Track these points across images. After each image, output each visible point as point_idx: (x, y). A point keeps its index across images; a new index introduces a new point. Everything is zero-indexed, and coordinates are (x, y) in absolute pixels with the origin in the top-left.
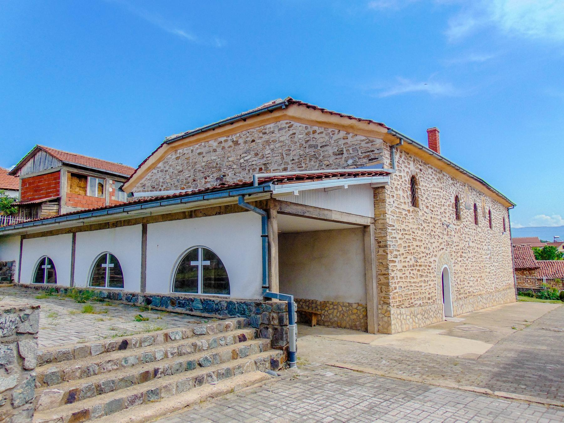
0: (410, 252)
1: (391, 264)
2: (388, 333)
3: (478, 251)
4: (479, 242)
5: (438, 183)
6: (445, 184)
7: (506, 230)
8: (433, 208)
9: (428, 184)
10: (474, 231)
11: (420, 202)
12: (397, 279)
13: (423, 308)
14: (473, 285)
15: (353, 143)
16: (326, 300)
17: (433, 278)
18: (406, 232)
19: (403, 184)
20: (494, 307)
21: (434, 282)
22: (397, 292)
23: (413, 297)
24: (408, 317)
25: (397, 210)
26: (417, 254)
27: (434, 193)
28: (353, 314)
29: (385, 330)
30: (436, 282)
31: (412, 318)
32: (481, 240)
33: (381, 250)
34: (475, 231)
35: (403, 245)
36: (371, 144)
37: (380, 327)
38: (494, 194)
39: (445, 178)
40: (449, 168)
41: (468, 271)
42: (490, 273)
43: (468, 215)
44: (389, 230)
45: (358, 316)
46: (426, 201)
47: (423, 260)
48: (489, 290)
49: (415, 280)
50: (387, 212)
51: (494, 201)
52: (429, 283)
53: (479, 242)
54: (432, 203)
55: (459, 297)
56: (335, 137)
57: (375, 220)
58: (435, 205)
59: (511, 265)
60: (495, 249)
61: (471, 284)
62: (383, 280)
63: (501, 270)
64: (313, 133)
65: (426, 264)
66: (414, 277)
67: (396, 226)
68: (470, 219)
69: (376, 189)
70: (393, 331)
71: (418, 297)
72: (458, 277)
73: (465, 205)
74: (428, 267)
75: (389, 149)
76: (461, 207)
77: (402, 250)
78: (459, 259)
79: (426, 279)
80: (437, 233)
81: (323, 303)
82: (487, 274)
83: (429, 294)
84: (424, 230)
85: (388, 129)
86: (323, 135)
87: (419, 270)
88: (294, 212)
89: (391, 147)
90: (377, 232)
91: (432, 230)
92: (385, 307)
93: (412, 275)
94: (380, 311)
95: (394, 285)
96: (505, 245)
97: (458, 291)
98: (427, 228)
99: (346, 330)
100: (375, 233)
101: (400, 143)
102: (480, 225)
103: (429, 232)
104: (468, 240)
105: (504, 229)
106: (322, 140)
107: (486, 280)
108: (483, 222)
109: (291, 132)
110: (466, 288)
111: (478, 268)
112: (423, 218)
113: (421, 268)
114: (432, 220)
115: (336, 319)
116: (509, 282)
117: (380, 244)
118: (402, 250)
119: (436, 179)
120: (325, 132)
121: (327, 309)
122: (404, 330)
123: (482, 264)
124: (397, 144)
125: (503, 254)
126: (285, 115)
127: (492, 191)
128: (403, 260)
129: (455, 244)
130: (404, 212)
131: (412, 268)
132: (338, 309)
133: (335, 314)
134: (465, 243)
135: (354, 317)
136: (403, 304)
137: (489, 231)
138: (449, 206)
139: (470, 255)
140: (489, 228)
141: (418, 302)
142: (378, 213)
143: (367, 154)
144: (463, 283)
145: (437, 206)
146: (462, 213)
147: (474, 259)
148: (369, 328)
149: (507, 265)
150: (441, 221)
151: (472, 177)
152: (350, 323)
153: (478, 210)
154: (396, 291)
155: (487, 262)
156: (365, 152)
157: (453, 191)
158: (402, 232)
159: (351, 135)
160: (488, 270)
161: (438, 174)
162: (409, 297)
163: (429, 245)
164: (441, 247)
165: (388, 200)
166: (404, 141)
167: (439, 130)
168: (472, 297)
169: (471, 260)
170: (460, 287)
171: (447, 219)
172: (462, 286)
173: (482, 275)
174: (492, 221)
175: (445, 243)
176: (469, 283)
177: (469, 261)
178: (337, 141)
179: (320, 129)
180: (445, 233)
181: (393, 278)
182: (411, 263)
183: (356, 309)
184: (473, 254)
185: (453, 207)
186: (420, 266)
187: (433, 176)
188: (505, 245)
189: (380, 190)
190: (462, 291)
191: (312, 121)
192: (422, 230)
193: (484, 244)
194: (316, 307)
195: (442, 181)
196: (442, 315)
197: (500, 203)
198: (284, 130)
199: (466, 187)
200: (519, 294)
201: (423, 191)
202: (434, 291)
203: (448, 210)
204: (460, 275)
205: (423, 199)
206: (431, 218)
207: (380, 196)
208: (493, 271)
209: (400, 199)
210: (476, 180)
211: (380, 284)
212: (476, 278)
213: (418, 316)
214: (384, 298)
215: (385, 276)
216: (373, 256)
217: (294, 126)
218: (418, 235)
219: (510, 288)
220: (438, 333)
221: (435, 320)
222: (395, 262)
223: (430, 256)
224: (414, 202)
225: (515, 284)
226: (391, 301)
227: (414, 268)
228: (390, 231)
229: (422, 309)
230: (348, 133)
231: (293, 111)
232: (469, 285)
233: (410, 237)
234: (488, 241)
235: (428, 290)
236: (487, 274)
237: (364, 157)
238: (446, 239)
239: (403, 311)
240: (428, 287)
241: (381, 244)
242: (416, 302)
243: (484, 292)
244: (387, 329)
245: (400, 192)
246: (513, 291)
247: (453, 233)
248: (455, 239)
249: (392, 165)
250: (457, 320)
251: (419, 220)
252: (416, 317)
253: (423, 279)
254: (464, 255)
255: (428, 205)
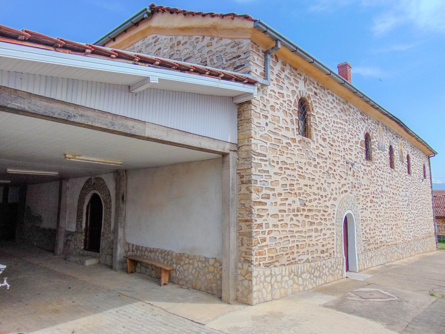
0: (293, 192)
1: (256, 207)
2: (248, 304)
3: (394, 196)
4: (394, 187)
5: (342, 114)
6: (351, 117)
7: (427, 178)
8: (334, 141)
9: (326, 112)
10: (389, 175)
11: (313, 133)
12: (268, 227)
13: (313, 264)
14: (387, 234)
15: (218, 49)
16: (182, 252)
17: (329, 226)
18: (288, 166)
19: (285, 105)
20: (411, 258)
21: (332, 231)
22: (267, 246)
23: (295, 250)
24: (286, 278)
25: (273, 136)
26: (305, 195)
27: (336, 125)
28: (209, 272)
29: (244, 299)
30: (335, 231)
31: (293, 279)
32: (397, 185)
33: (244, 187)
34: (391, 175)
35: (281, 182)
36: (237, 47)
37: (239, 294)
38: (413, 139)
39: (352, 110)
40: (355, 99)
41: (381, 219)
42: (407, 220)
43: (381, 157)
44: (256, 160)
45: (215, 276)
46: (323, 132)
47: (314, 203)
48: (406, 239)
49: (300, 229)
50: (253, 135)
51: (414, 147)
52: (324, 232)
53: (394, 187)
54: (331, 136)
55: (368, 248)
56: (199, 46)
57: (238, 148)
58: (336, 138)
59: (431, 212)
60: (413, 196)
61: (384, 232)
62: (245, 229)
63: (421, 218)
64: (178, 45)
65: (319, 208)
66: (300, 225)
67: (270, 156)
68: (385, 162)
69: (241, 105)
70: (255, 302)
71: (305, 250)
72: (367, 225)
73: (378, 144)
74: (322, 212)
75: (261, 54)
76: (373, 146)
77: (279, 189)
78: (369, 204)
79: (319, 228)
80: (338, 172)
81: (178, 255)
82: (404, 222)
83: (323, 246)
84: (318, 166)
85: (255, 21)
86: (187, 46)
87: (307, 216)
88: (41, 111)
89: (266, 53)
90: (240, 162)
91: (331, 168)
92: (246, 266)
93: (294, 222)
94: (239, 271)
95: (261, 236)
96: (425, 193)
97: (367, 241)
98: (322, 164)
99: (199, 294)
100: (238, 164)
101: (276, 46)
102: (396, 169)
103: (326, 169)
104: (382, 183)
105: (425, 176)
106: (186, 52)
107: (402, 228)
108: (400, 166)
109: (157, 48)
110: (376, 237)
111: (392, 215)
112: (317, 152)
113: (310, 214)
114: (331, 156)
115: (191, 277)
116: (430, 230)
117: (243, 179)
118: (279, 189)
119: (339, 109)
120: (189, 41)
121: (182, 263)
122: (277, 296)
123: (398, 211)
124: (273, 48)
125: (423, 201)
126: (150, 28)
127: (410, 134)
128: (279, 202)
129: (363, 187)
130: (285, 141)
131: (296, 213)
132: (193, 265)
133: (190, 270)
134: (377, 187)
135: (210, 276)
136: (277, 261)
137: (407, 177)
138: (357, 143)
139: (384, 201)
140: (407, 174)
141: (305, 258)
142: (242, 137)
143: (232, 61)
144: (373, 231)
145: (339, 140)
146: (373, 153)
147: (388, 206)
148: (224, 295)
149: (427, 213)
150: (344, 158)
151: (386, 115)
152: (205, 284)
153: (395, 153)
154: (264, 244)
155: (404, 209)
156: (231, 60)
157: (361, 128)
158: (280, 165)
159: (216, 39)
160: (406, 218)
161: (342, 104)
162: (289, 251)
163: (325, 186)
164: (343, 189)
165: (255, 120)
166: (283, 44)
167: (351, 66)
168: (385, 247)
169: (385, 206)
170: (369, 236)
171: (353, 158)
172: (372, 235)
173: (398, 222)
174: (411, 167)
175: (350, 185)
176: (381, 232)
177: (381, 207)
178: (200, 51)
179: (184, 38)
180: (351, 173)
181: (260, 226)
182: (294, 206)
183: (213, 265)
184: (388, 199)
185: (362, 145)
186: (310, 210)
187: (335, 104)
188: (425, 193)
189: (245, 106)
190: (372, 241)
191: (175, 29)
192: (315, 166)
193: (400, 190)
194: (172, 260)
195: (347, 113)
196: (342, 271)
197: (420, 149)
198: (151, 47)
199: (380, 126)
200: (440, 241)
201: (318, 120)
202: (332, 243)
203: (354, 147)
204: (369, 222)
205: (318, 129)
206: (330, 153)
207: (246, 115)
208: (411, 219)
209: (278, 121)
210: (391, 118)
211: (240, 234)
212: (391, 226)
213: (304, 276)
214: (246, 253)
215: (248, 223)
216: (231, 195)
217: (159, 40)
218: (307, 172)
219: (430, 237)
220: (324, 302)
221: (331, 278)
222: (265, 204)
223: (327, 199)
224: (305, 131)
225: (435, 232)
226: (254, 258)
227: (299, 213)
228: (256, 161)
229: (310, 266)
230: (212, 38)
231: (158, 21)
232: (381, 234)
233: (295, 173)
234: (405, 186)
235: (321, 240)
236: (404, 222)
237: (229, 66)
238: (351, 180)
239: (277, 270)
240: (322, 237)
241: (244, 179)
242: (300, 258)
243: (400, 241)
244: (246, 297)
245: (281, 114)
246: (434, 238)
247: (361, 174)
248: (363, 182)
249: (265, 75)
250: (361, 277)
251: (311, 154)
252: (298, 276)
253: (314, 227)
254: (375, 200)
255: (326, 137)
